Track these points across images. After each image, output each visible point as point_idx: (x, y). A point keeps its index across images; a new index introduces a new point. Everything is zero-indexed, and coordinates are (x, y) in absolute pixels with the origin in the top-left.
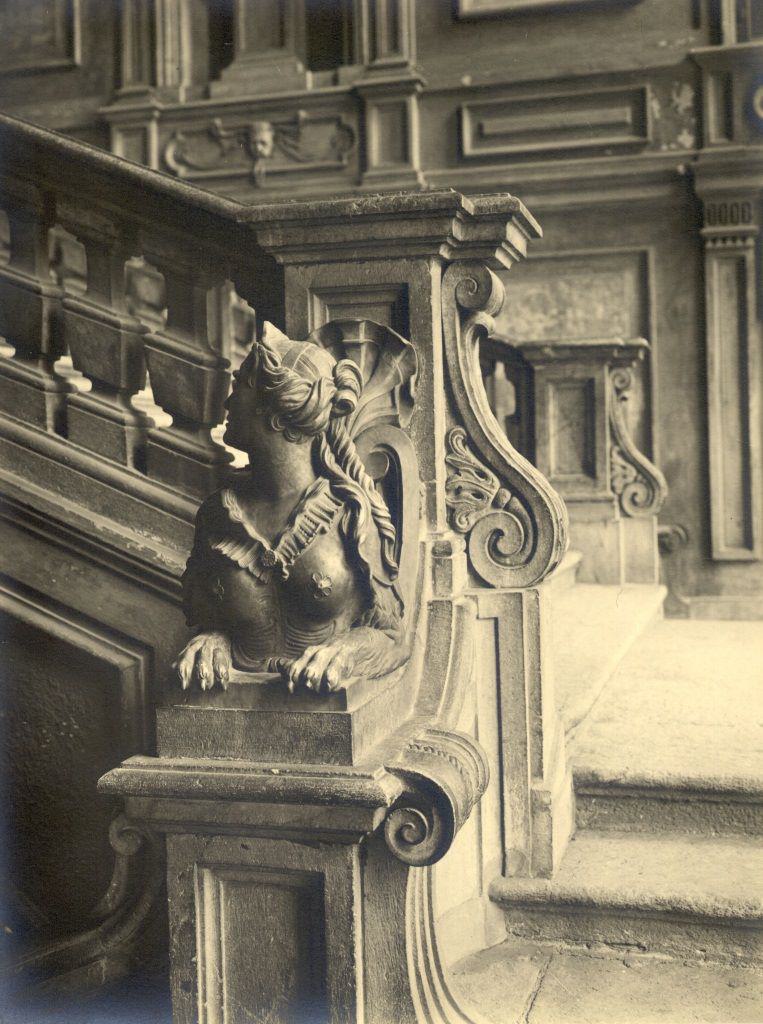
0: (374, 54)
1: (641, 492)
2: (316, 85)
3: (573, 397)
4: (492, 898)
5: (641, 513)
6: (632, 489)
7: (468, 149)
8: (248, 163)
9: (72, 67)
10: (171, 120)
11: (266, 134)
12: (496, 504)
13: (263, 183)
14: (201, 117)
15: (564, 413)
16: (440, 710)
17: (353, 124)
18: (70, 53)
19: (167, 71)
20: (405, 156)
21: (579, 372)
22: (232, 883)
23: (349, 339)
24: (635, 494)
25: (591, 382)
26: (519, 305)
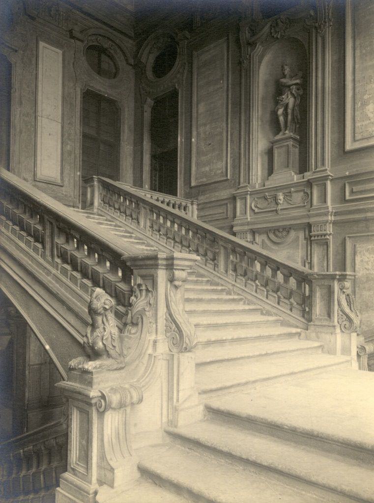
0: (316, 167)
1: (348, 324)
2: (297, 180)
3: (325, 291)
4: (165, 431)
5: (347, 332)
6: (344, 323)
7: (347, 198)
8: (276, 206)
9: (228, 180)
10: (254, 194)
11: (281, 197)
12: (174, 331)
13: (280, 212)
14: (261, 193)
15: (322, 296)
16: (141, 381)
17: (309, 192)
18: (227, 176)
19: (253, 178)
20: (325, 202)
21: (326, 282)
22: (80, 411)
23: (141, 288)
24: (346, 325)
25: (330, 286)
26: (364, 252)
